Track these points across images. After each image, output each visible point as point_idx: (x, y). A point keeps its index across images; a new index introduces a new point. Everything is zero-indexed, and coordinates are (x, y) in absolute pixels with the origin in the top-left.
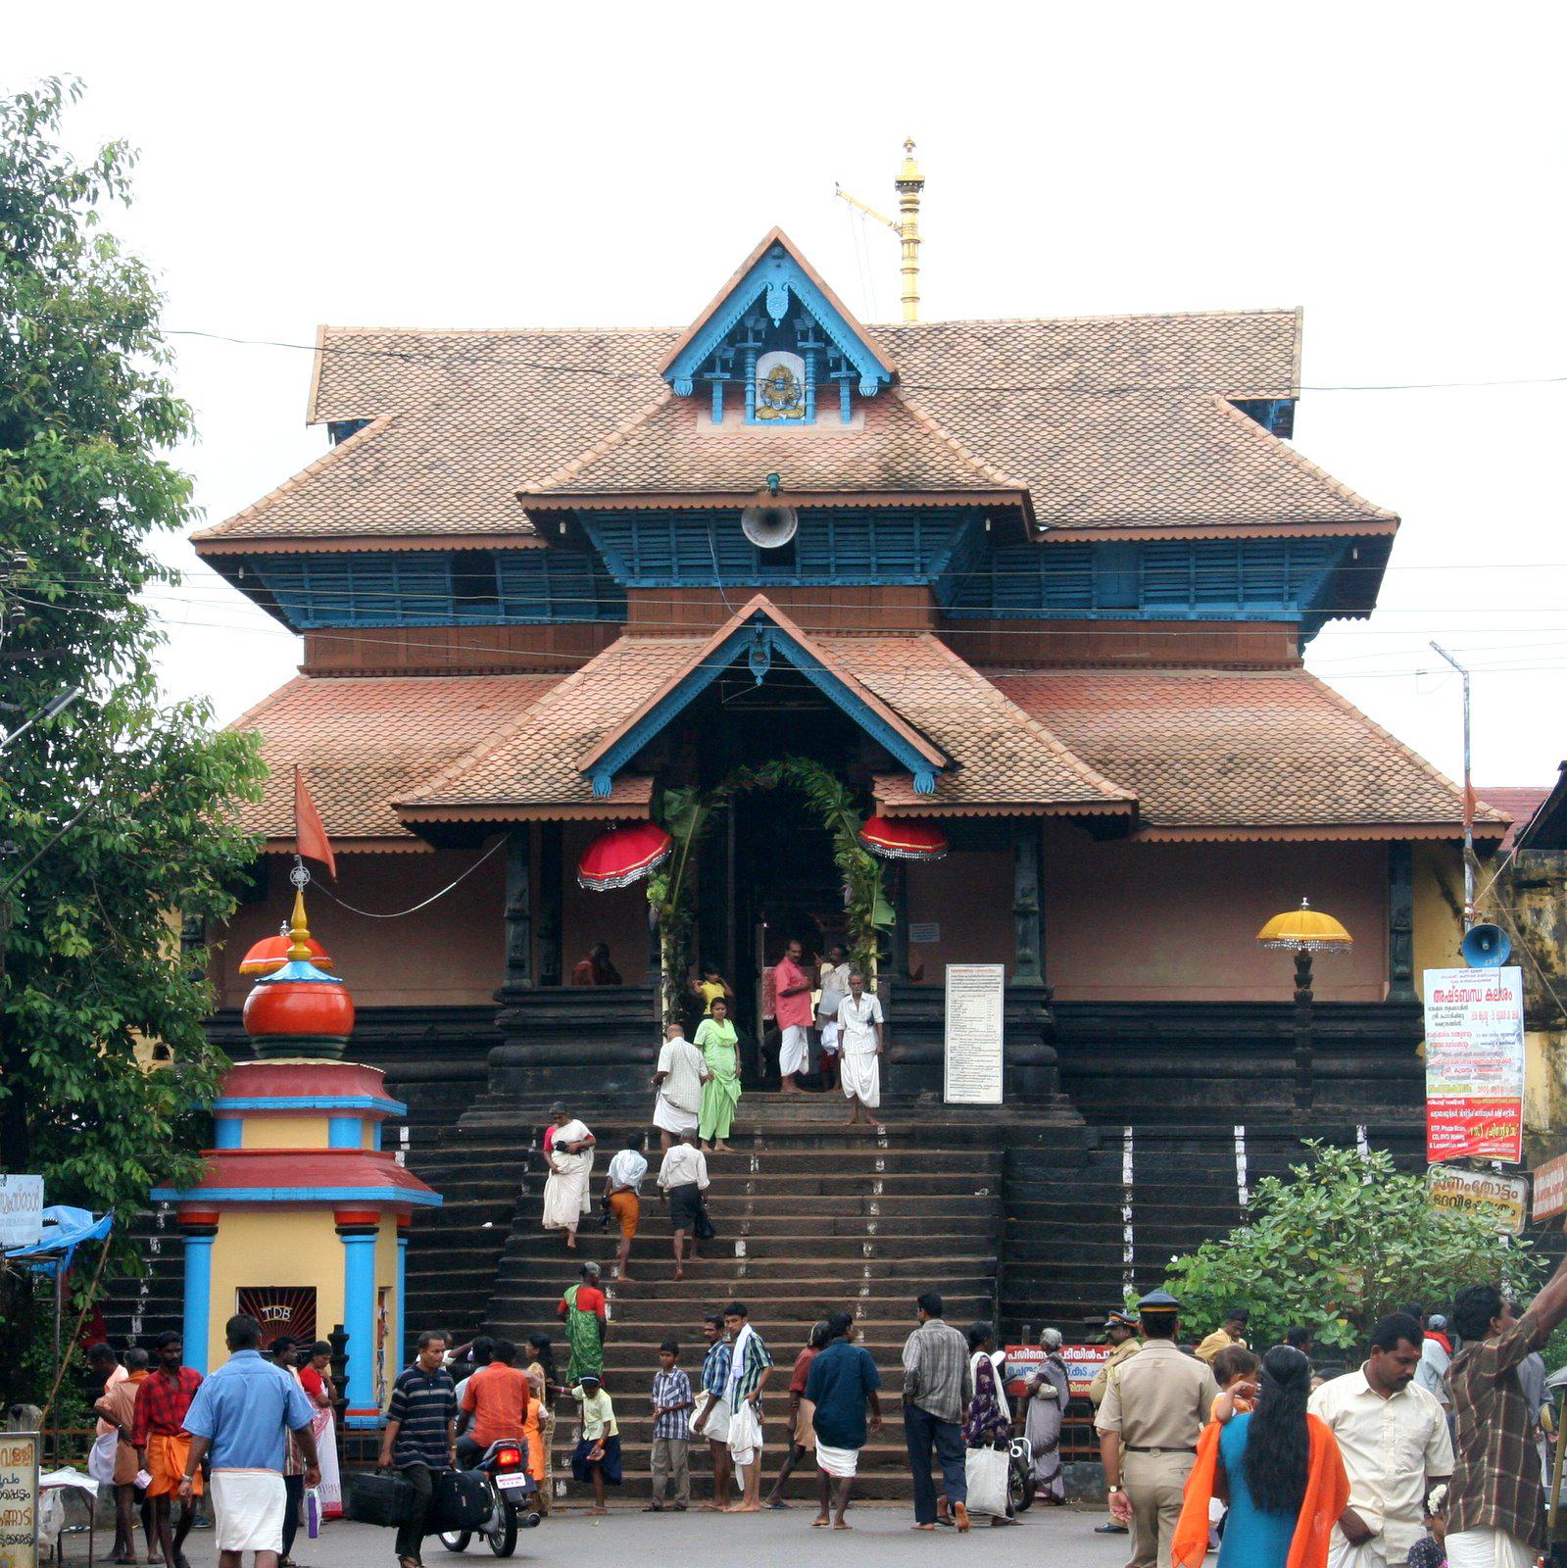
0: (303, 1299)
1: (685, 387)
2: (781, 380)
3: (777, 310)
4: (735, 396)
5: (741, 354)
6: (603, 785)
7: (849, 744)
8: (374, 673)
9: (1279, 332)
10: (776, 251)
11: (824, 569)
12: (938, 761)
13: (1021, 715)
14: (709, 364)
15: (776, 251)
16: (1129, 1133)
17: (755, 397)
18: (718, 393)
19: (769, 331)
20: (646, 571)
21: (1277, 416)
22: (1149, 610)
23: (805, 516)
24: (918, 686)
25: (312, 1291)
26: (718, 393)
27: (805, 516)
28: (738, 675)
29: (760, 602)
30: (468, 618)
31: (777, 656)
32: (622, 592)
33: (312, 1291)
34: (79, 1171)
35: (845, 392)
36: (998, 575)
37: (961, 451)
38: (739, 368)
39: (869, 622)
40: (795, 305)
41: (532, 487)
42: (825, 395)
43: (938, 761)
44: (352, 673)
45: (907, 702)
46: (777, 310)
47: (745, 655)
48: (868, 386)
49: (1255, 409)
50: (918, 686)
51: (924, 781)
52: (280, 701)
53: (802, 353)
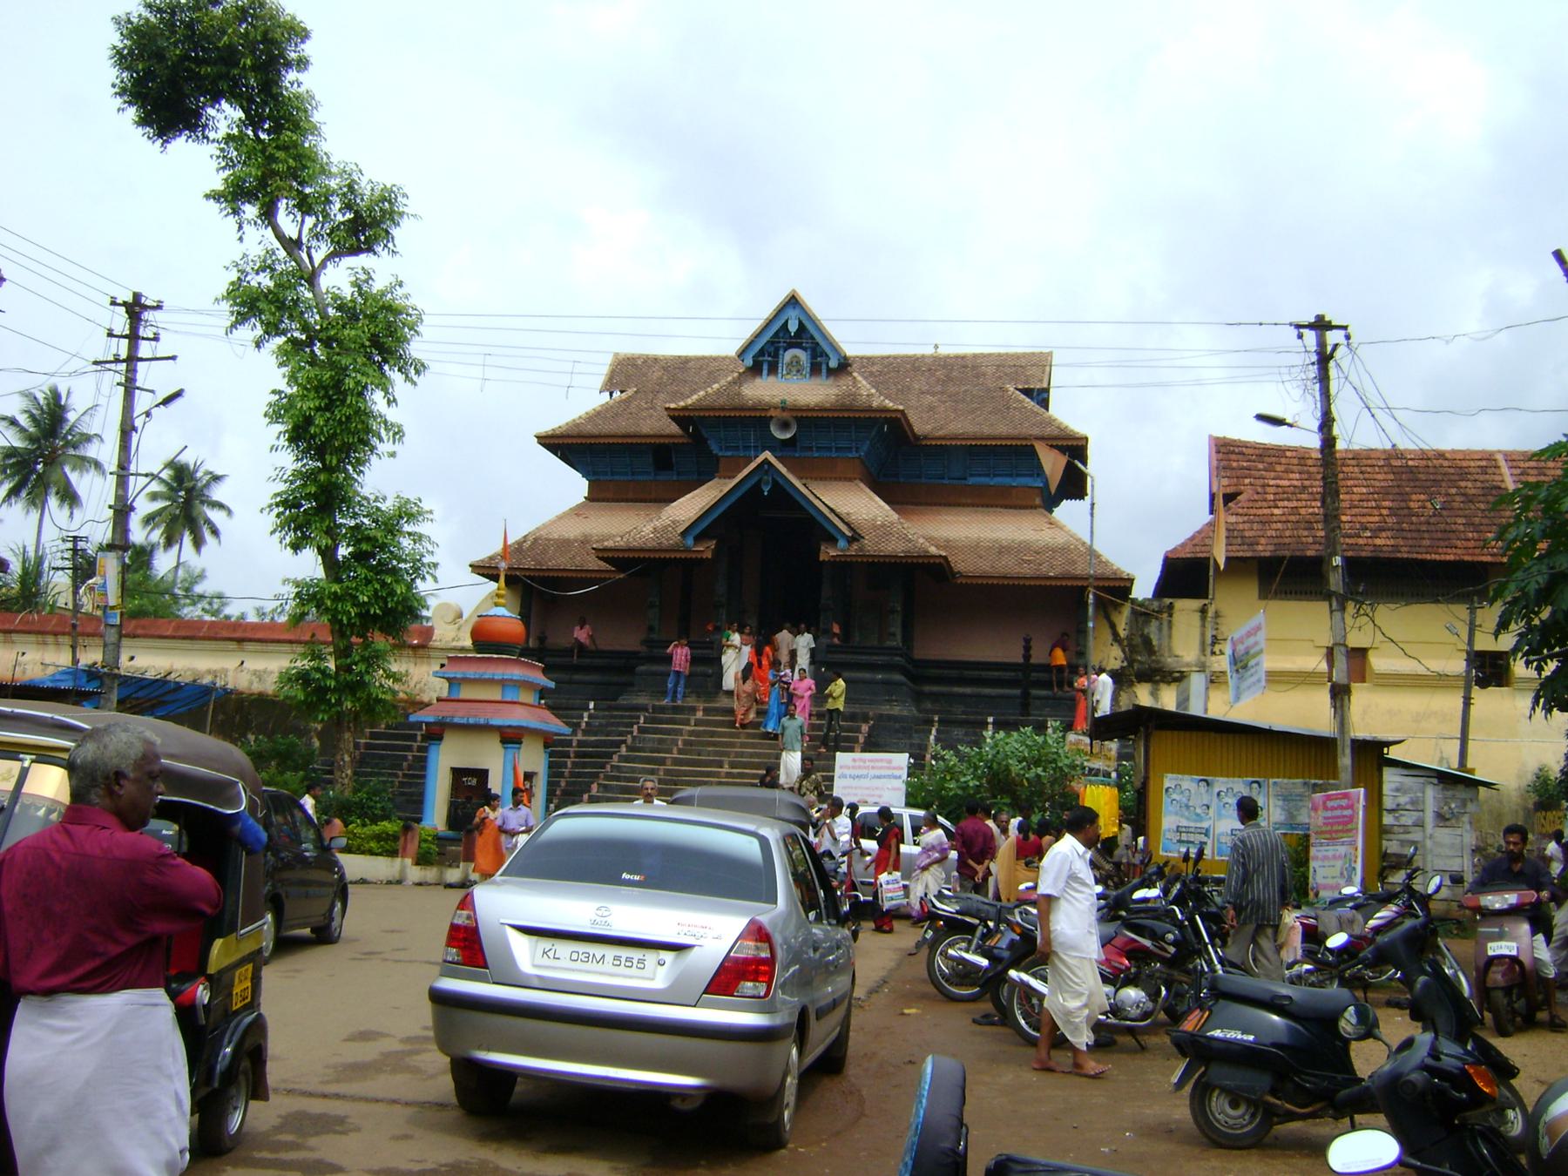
0: (482, 775)
1: (749, 362)
2: (795, 362)
3: (793, 327)
4: (773, 369)
5: (777, 350)
6: (690, 541)
7: (813, 527)
8: (618, 501)
9: (1041, 362)
10: (793, 301)
11: (810, 449)
12: (849, 534)
13: (896, 516)
14: (761, 352)
15: (793, 301)
16: (990, 720)
17: (783, 369)
18: (765, 367)
19: (790, 337)
20: (727, 448)
21: (1041, 397)
22: (971, 481)
23: (799, 420)
24: (854, 505)
25: (486, 772)
26: (765, 367)
27: (799, 420)
28: (757, 488)
29: (767, 455)
30: (662, 477)
31: (775, 484)
32: (717, 458)
33: (486, 772)
34: (1548, 852)
35: (824, 367)
36: (899, 455)
37: (866, 391)
38: (776, 355)
39: (830, 473)
40: (801, 326)
41: (673, 406)
42: (815, 370)
43: (849, 534)
44: (608, 500)
45: (842, 509)
46: (793, 327)
47: (759, 481)
48: (833, 364)
49: (1027, 392)
50: (854, 505)
51: (842, 543)
52: (577, 511)
53: (805, 349)
